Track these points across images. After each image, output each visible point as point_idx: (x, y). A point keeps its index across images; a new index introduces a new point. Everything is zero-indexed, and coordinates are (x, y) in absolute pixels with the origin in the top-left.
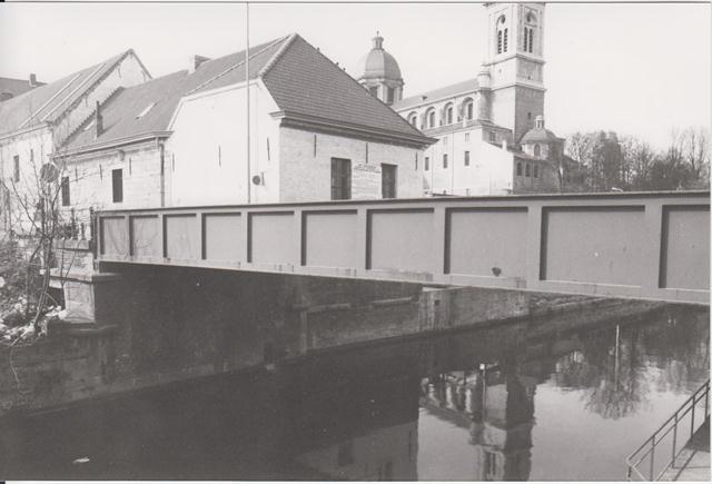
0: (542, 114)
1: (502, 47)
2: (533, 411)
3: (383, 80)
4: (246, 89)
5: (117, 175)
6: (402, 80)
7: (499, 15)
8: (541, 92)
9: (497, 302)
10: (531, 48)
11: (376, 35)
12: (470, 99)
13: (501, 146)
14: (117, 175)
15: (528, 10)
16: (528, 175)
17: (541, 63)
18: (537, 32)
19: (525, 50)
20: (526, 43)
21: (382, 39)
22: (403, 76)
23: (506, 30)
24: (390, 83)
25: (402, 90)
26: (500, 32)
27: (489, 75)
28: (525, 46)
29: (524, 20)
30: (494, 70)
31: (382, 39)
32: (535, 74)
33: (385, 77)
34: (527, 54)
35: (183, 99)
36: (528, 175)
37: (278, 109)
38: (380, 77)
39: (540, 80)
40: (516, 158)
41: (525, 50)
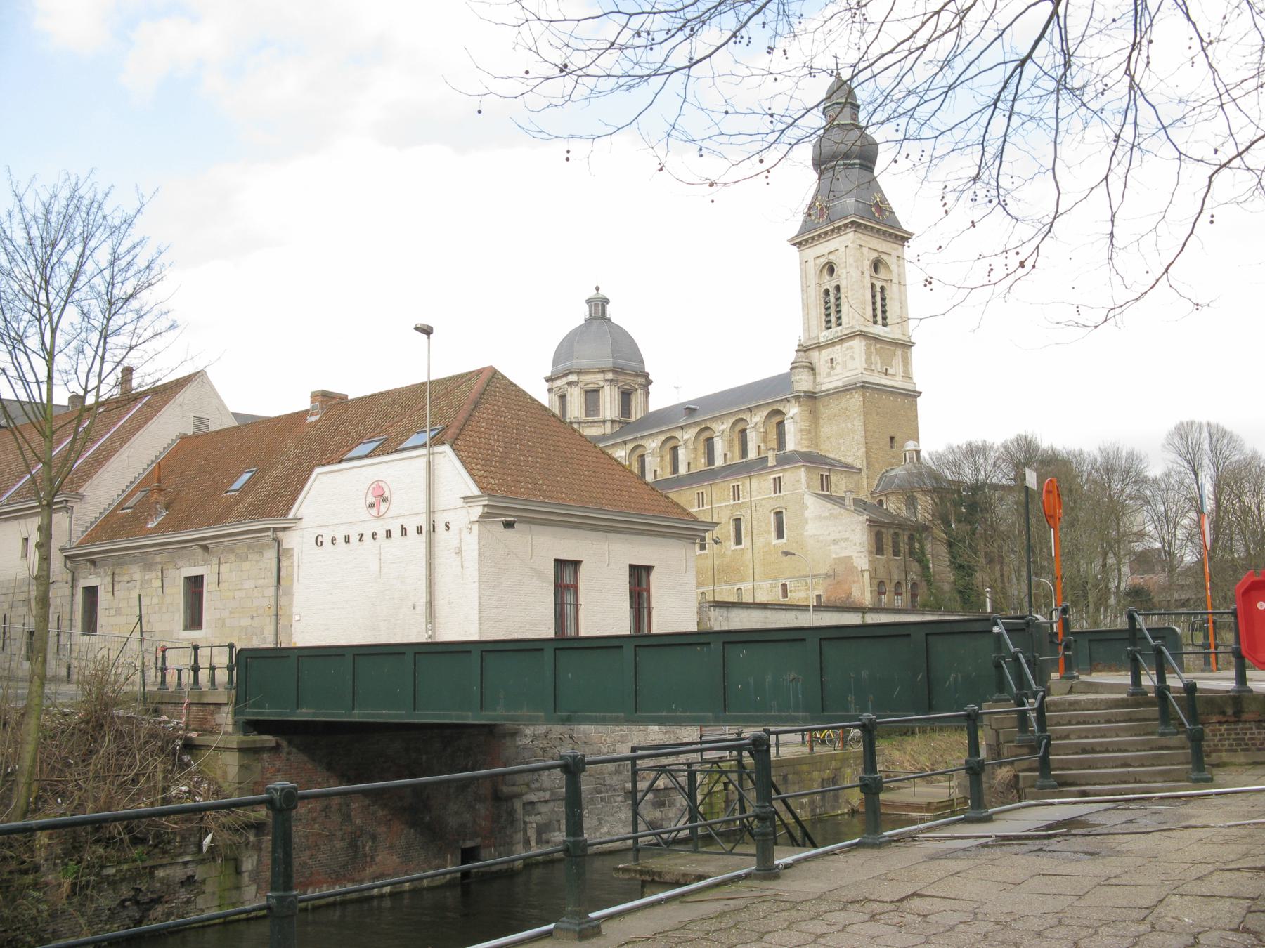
0: (917, 440)
1: (833, 319)
2: (343, 398)
3: (610, 376)
4: (424, 461)
5: (195, 585)
6: (646, 376)
7: (823, 261)
8: (912, 396)
9: (1223, 556)
10: (884, 318)
11: (592, 293)
12: (779, 412)
13: (839, 501)
14: (195, 585)
15: (875, 255)
16: (896, 553)
17: (907, 346)
18: (892, 291)
19: (875, 323)
20: (874, 310)
21: (605, 301)
22: (648, 369)
23: (838, 288)
24: (626, 380)
25: (647, 393)
26: (827, 292)
27: (813, 369)
28: (875, 316)
29: (868, 272)
30: (820, 359)
31: (605, 301)
32: (897, 368)
33: (614, 372)
34: (878, 330)
35: (318, 470)
36: (896, 553)
37: (476, 492)
38: (602, 371)
39: (907, 376)
40: (872, 523)
41: (882, 288)
